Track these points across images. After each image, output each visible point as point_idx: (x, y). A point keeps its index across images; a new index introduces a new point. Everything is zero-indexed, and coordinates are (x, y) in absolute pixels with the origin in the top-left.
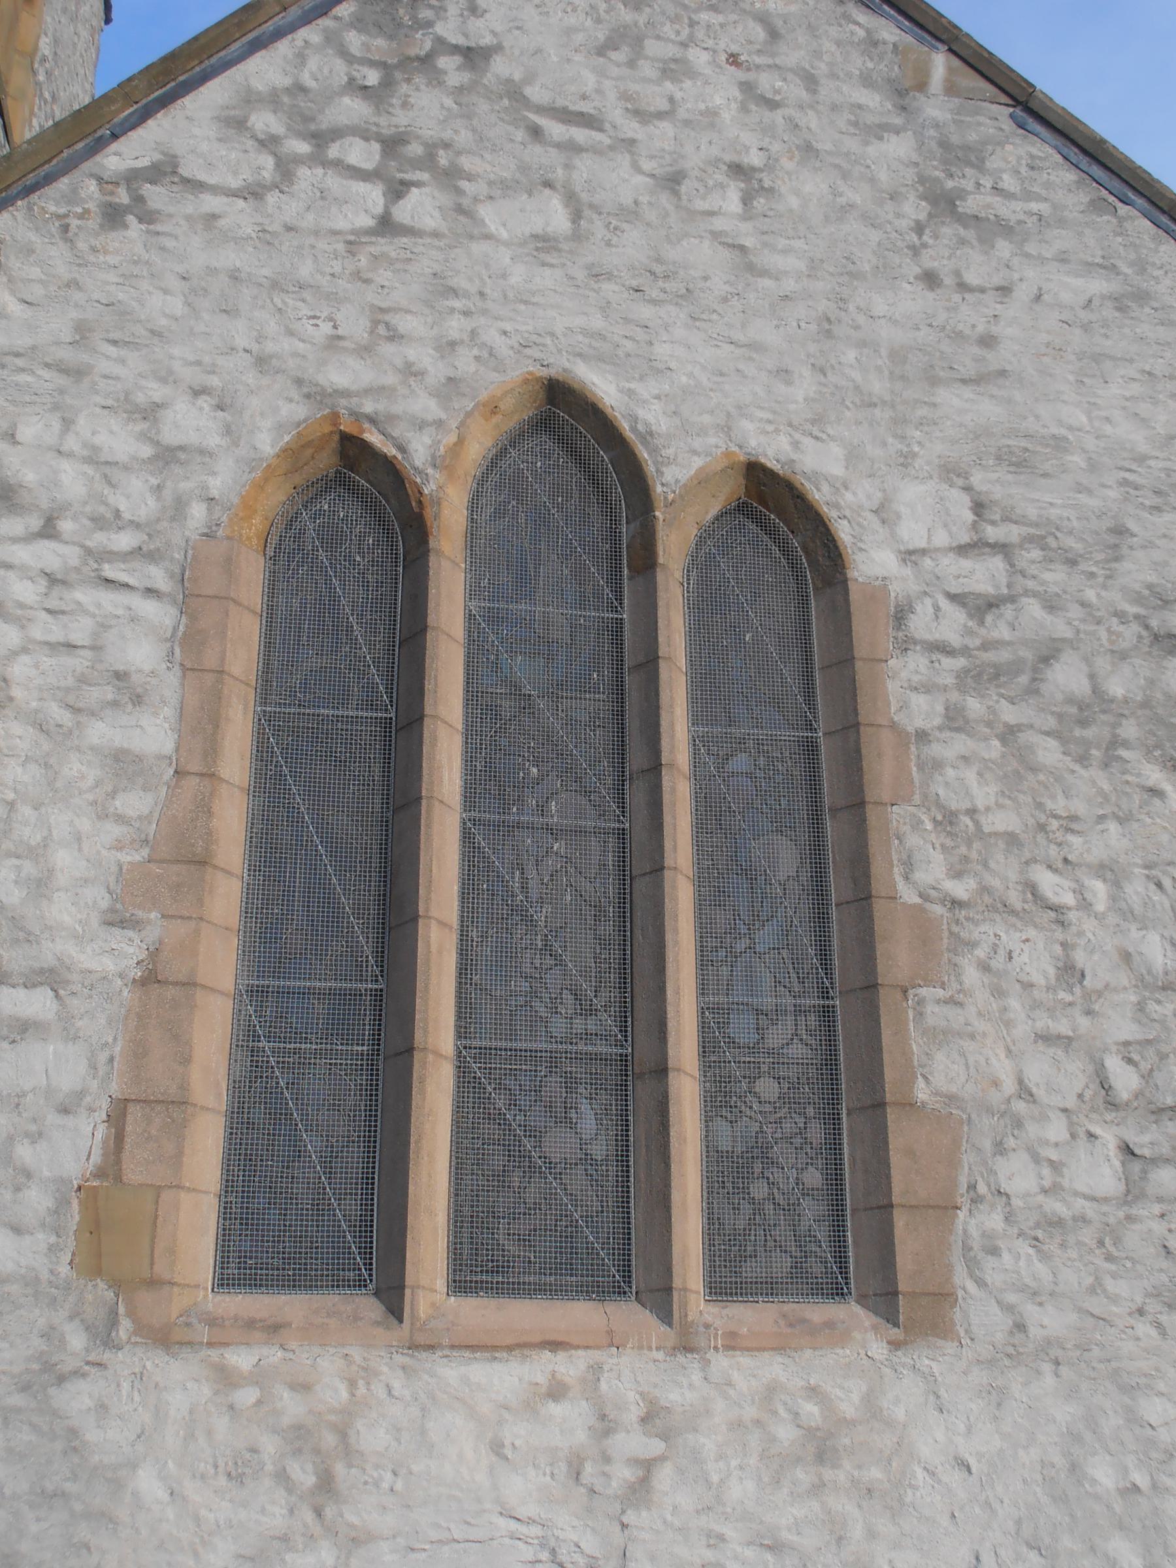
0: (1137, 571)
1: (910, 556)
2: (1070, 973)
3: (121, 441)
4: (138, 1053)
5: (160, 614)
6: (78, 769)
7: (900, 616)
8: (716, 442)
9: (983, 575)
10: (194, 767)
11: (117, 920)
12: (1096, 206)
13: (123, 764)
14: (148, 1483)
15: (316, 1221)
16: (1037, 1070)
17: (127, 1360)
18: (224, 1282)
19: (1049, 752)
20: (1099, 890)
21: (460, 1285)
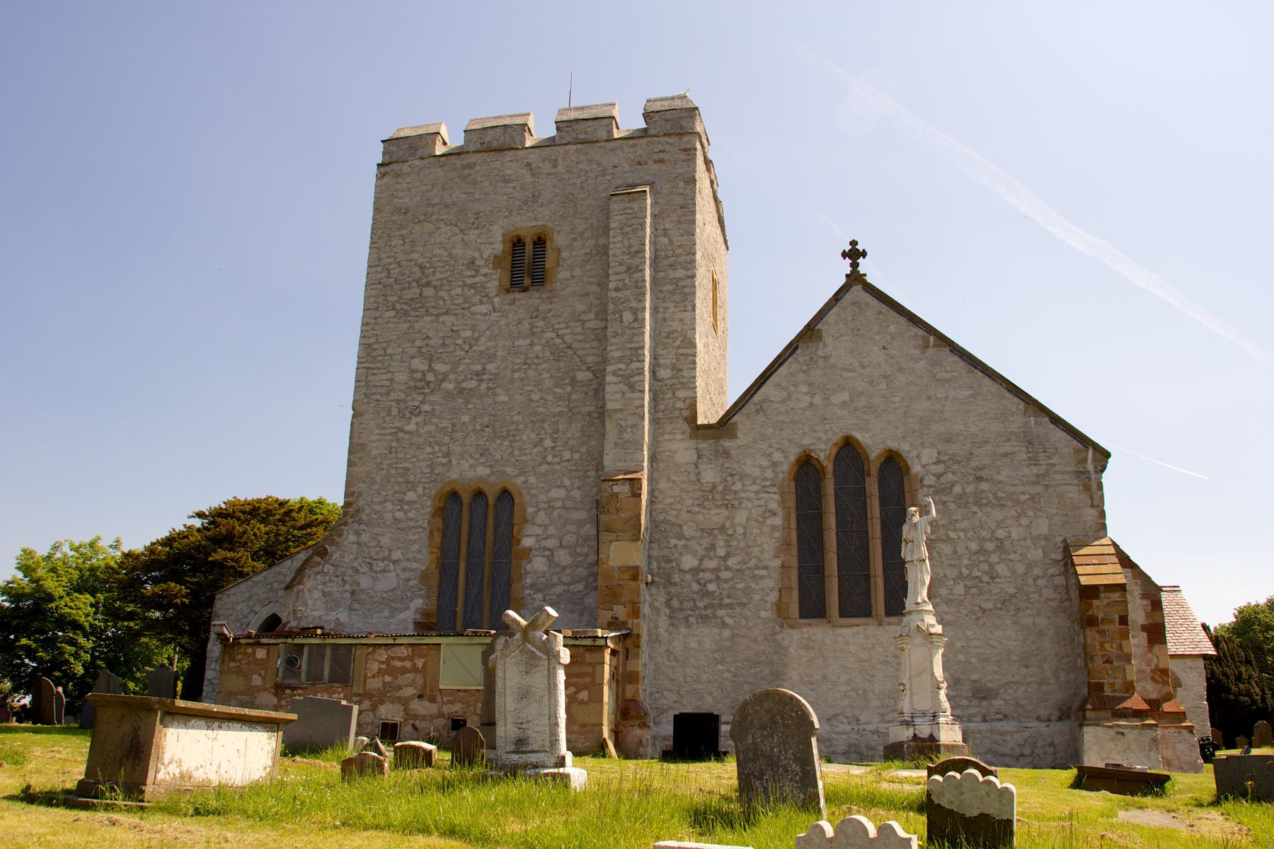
0: (974, 464)
1: (924, 466)
2: (955, 552)
3: (765, 463)
4: (782, 580)
5: (776, 497)
6: (767, 530)
7: (921, 481)
8: (882, 446)
9: (939, 469)
10: (786, 527)
11: (775, 557)
12: (969, 372)
13: (774, 528)
14: (791, 649)
15: (813, 608)
16: (947, 572)
17: (787, 631)
18: (801, 617)
19: (952, 506)
20: (962, 534)
21: (841, 616)
